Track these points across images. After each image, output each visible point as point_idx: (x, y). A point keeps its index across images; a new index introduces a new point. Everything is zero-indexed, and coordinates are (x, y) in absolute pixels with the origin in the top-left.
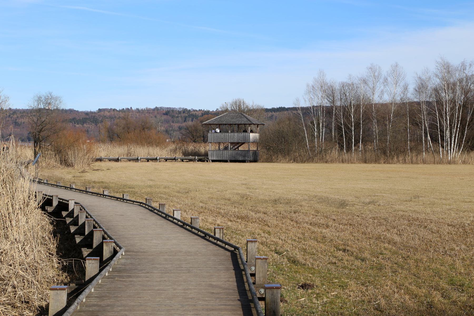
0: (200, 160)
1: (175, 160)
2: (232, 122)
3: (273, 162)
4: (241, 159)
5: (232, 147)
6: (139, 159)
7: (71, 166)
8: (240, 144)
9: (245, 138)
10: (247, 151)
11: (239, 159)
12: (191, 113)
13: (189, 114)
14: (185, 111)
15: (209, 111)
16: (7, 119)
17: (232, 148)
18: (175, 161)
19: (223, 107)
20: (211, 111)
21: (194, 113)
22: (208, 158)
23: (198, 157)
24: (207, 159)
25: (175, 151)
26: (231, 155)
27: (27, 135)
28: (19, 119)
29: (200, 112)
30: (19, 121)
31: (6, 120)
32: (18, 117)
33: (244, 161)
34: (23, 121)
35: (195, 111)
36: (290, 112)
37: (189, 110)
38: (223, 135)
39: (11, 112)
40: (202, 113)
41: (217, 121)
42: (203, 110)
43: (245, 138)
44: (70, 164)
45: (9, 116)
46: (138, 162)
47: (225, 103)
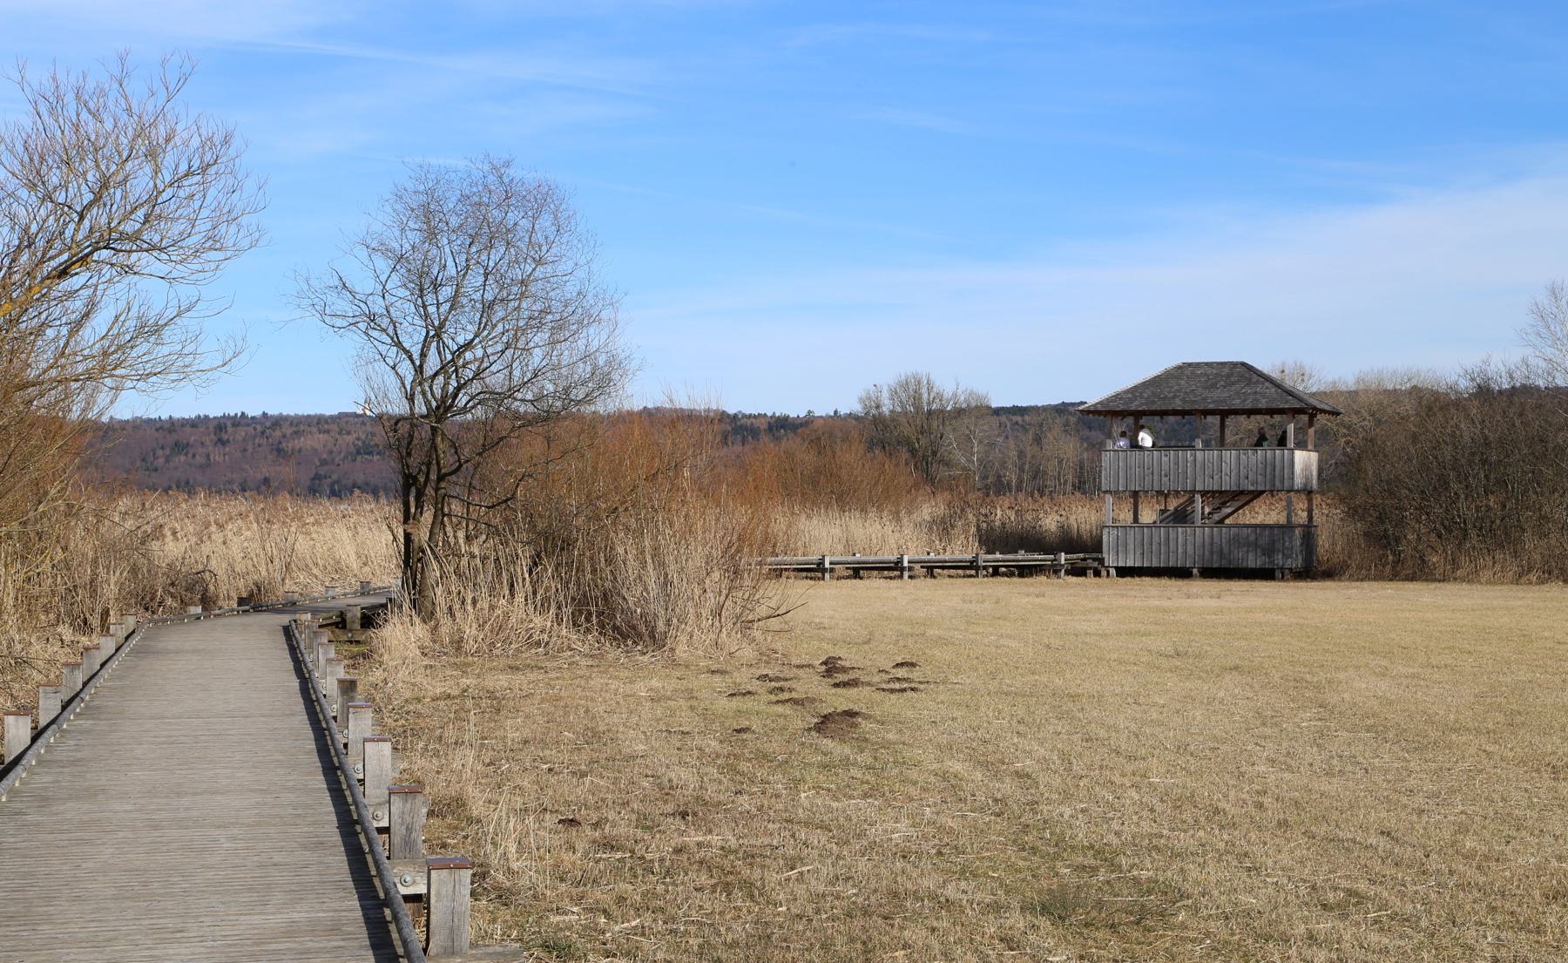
0: (1077, 571)
1: (977, 568)
2: (1213, 402)
3: (1435, 580)
4: (1252, 561)
5: (1207, 510)
6: (827, 565)
7: (640, 636)
8: (1245, 499)
9: (1270, 468)
10: (1281, 527)
11: (1244, 565)
12: (738, 423)
13: (736, 423)
14: (723, 416)
15: (788, 416)
16: (257, 441)
17: (1209, 514)
18: (973, 572)
19: (869, 398)
20: (791, 416)
21: (749, 422)
22: (1101, 561)
23: (1069, 556)
24: (1096, 564)
25: (943, 527)
26: (1207, 547)
27: (308, 483)
28: (288, 442)
29: (763, 421)
30: (287, 447)
31: (254, 444)
32: (284, 436)
33: (1266, 574)
34: (298, 447)
35: (744, 416)
36: (1003, 418)
37: (735, 415)
38: (1167, 458)
39: (268, 424)
40: (769, 423)
41: (1143, 397)
42: (769, 414)
43: (1270, 468)
44: (634, 628)
45: (263, 433)
46: (823, 579)
47: (875, 385)
